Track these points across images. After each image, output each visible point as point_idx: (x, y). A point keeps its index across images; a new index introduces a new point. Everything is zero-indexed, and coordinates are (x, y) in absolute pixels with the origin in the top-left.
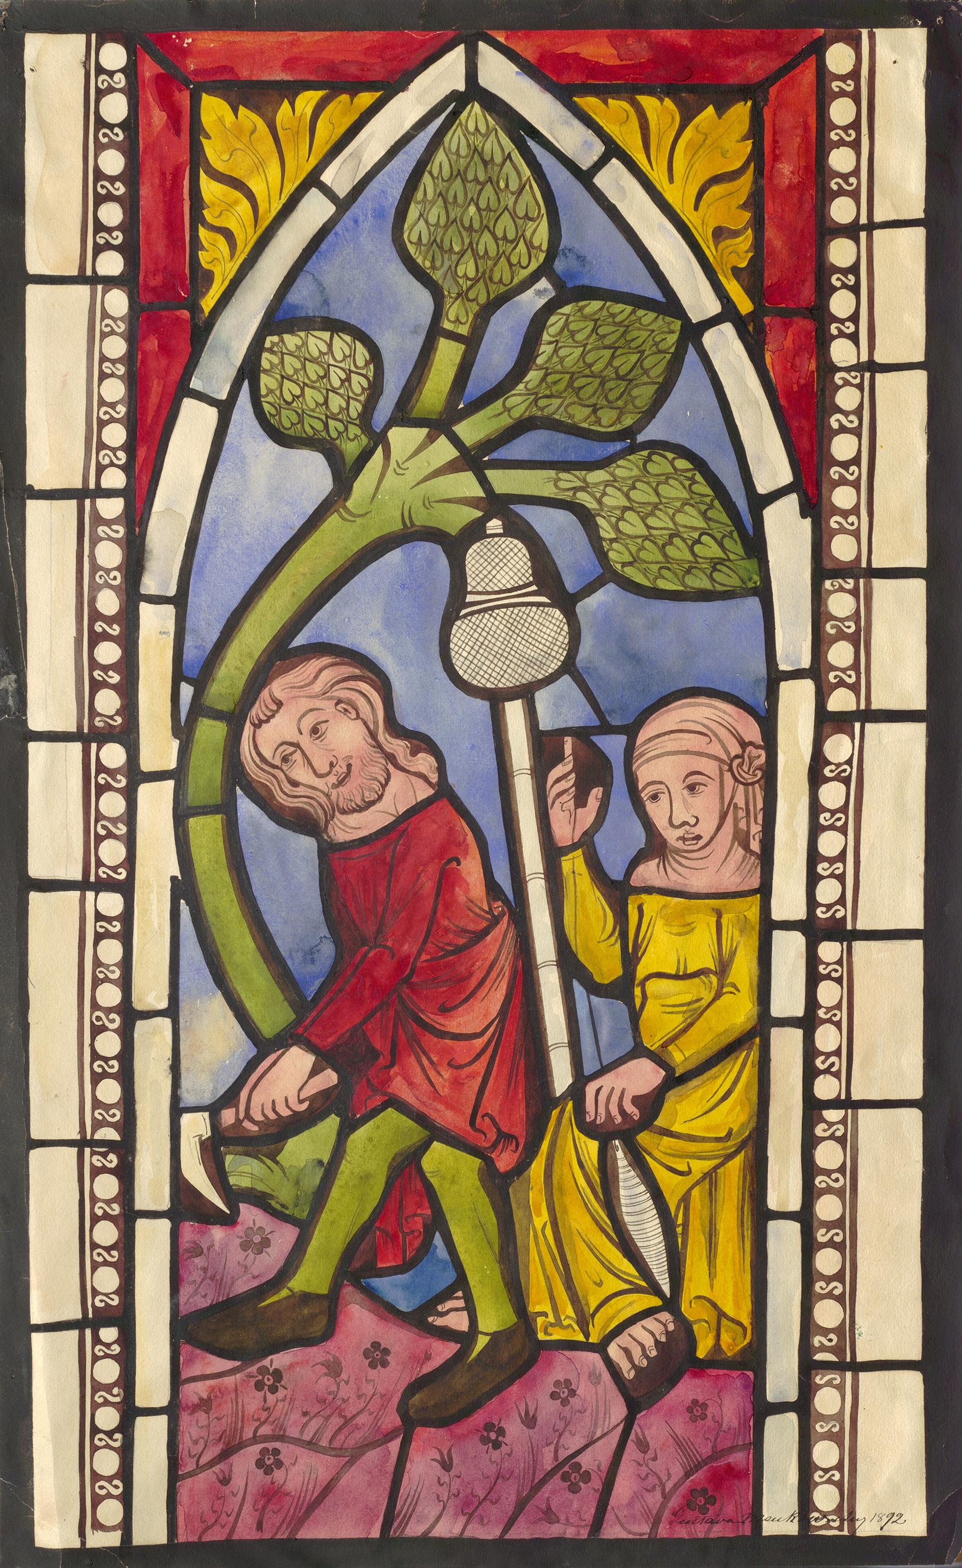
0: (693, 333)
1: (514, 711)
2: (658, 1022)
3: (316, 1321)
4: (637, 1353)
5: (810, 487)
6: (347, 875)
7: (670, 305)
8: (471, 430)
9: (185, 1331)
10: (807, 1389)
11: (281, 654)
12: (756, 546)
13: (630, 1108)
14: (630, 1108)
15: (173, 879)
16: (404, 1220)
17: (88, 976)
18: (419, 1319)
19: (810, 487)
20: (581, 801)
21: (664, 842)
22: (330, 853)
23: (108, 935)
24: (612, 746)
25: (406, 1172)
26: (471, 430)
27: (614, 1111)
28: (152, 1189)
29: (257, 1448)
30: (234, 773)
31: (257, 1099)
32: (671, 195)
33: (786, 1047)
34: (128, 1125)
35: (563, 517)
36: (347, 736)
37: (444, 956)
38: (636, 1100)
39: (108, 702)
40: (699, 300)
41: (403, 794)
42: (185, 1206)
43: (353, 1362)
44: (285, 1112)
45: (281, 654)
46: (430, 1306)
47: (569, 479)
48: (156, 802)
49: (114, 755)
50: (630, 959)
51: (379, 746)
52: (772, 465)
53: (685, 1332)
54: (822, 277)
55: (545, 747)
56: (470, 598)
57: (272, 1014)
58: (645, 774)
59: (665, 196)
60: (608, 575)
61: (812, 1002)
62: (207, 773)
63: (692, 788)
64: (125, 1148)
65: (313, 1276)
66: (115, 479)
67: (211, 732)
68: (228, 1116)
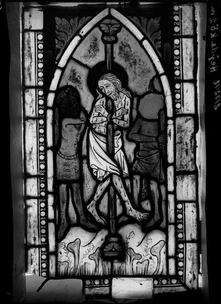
66: (41, 83)
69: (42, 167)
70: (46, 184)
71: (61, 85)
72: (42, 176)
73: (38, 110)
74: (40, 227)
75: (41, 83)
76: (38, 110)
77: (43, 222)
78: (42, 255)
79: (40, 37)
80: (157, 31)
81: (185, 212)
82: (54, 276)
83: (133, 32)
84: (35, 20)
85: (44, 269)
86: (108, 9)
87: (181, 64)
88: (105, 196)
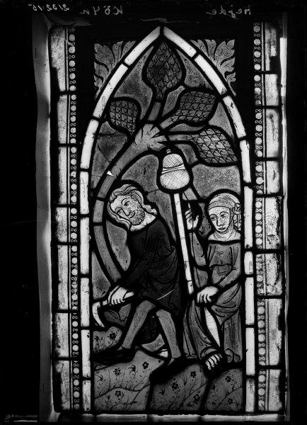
0: (219, 98)
1: (177, 197)
2: (216, 278)
3: (127, 356)
4: (216, 361)
5: (250, 137)
6: (133, 239)
7: (214, 90)
8: (165, 125)
9: (94, 357)
10: (257, 375)
11: (118, 183)
12: (238, 152)
13: (209, 300)
14: (209, 300)
15: (59, 347)
16: (151, 329)
17: (71, 267)
18: (155, 354)
19: (250, 137)
20: (194, 219)
21: (215, 229)
22: (130, 234)
23: (74, 256)
24: (202, 205)
25: (152, 313)
26: (165, 125)
27: (205, 300)
28: (85, 321)
29: (115, 390)
30: (106, 215)
31: (114, 298)
32: (215, 63)
33: (249, 283)
34: (79, 306)
35: (188, 147)
36: (133, 206)
37: (201, 131)
38: (210, 297)
39: (74, 199)
40: (220, 87)
41: (149, 219)
42: (93, 326)
43: (139, 367)
44: (119, 302)
45: (118, 183)
46: (160, 351)
47: (189, 137)
48: (85, 223)
49: (74, 211)
50: (208, 261)
51: (142, 207)
52: (241, 131)
53: (225, 356)
54: (252, 84)
55: (184, 204)
56: (164, 169)
57: (116, 275)
58: (211, 212)
59: (212, 68)
60: (201, 161)
61: (255, 269)
62: (98, 218)
63: (222, 216)
64: (79, 312)
65: (127, 343)
66: (73, 141)
67: (99, 205)
68: (105, 303)
69: (76, 348)
70: (81, 368)
71: (116, 96)
72: (75, 311)
73: (71, 185)
74: (70, 283)
75: (73, 141)
76: (71, 185)
77: (76, 383)
78: (71, 127)
79: (74, 97)
80: (232, 57)
81: (266, 186)
82: (184, 198)
83: (204, 70)
84: (57, 54)
85: (77, 387)
86: (115, 281)
87: (263, 56)
88: (231, 130)
